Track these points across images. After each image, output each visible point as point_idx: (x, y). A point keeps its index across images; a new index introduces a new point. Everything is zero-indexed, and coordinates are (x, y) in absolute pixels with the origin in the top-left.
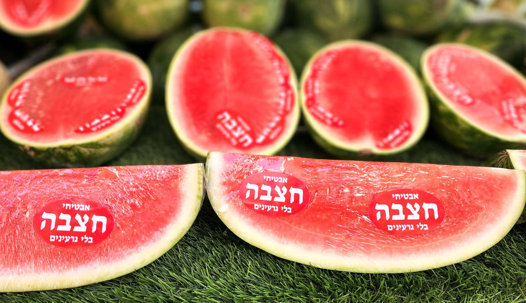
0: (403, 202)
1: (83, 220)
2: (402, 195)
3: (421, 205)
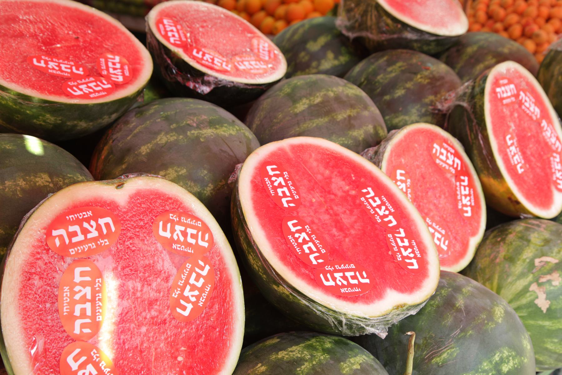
0: (79, 222)
2: (76, 215)
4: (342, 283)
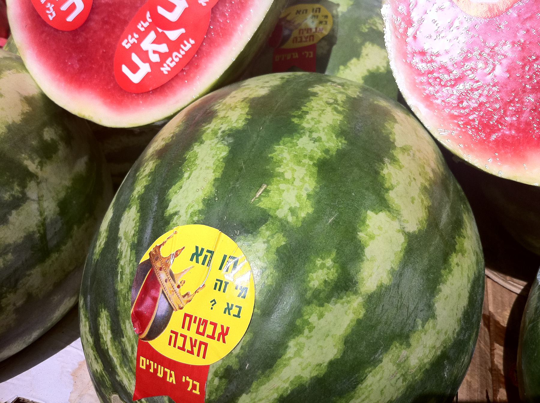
1: (155, 52)
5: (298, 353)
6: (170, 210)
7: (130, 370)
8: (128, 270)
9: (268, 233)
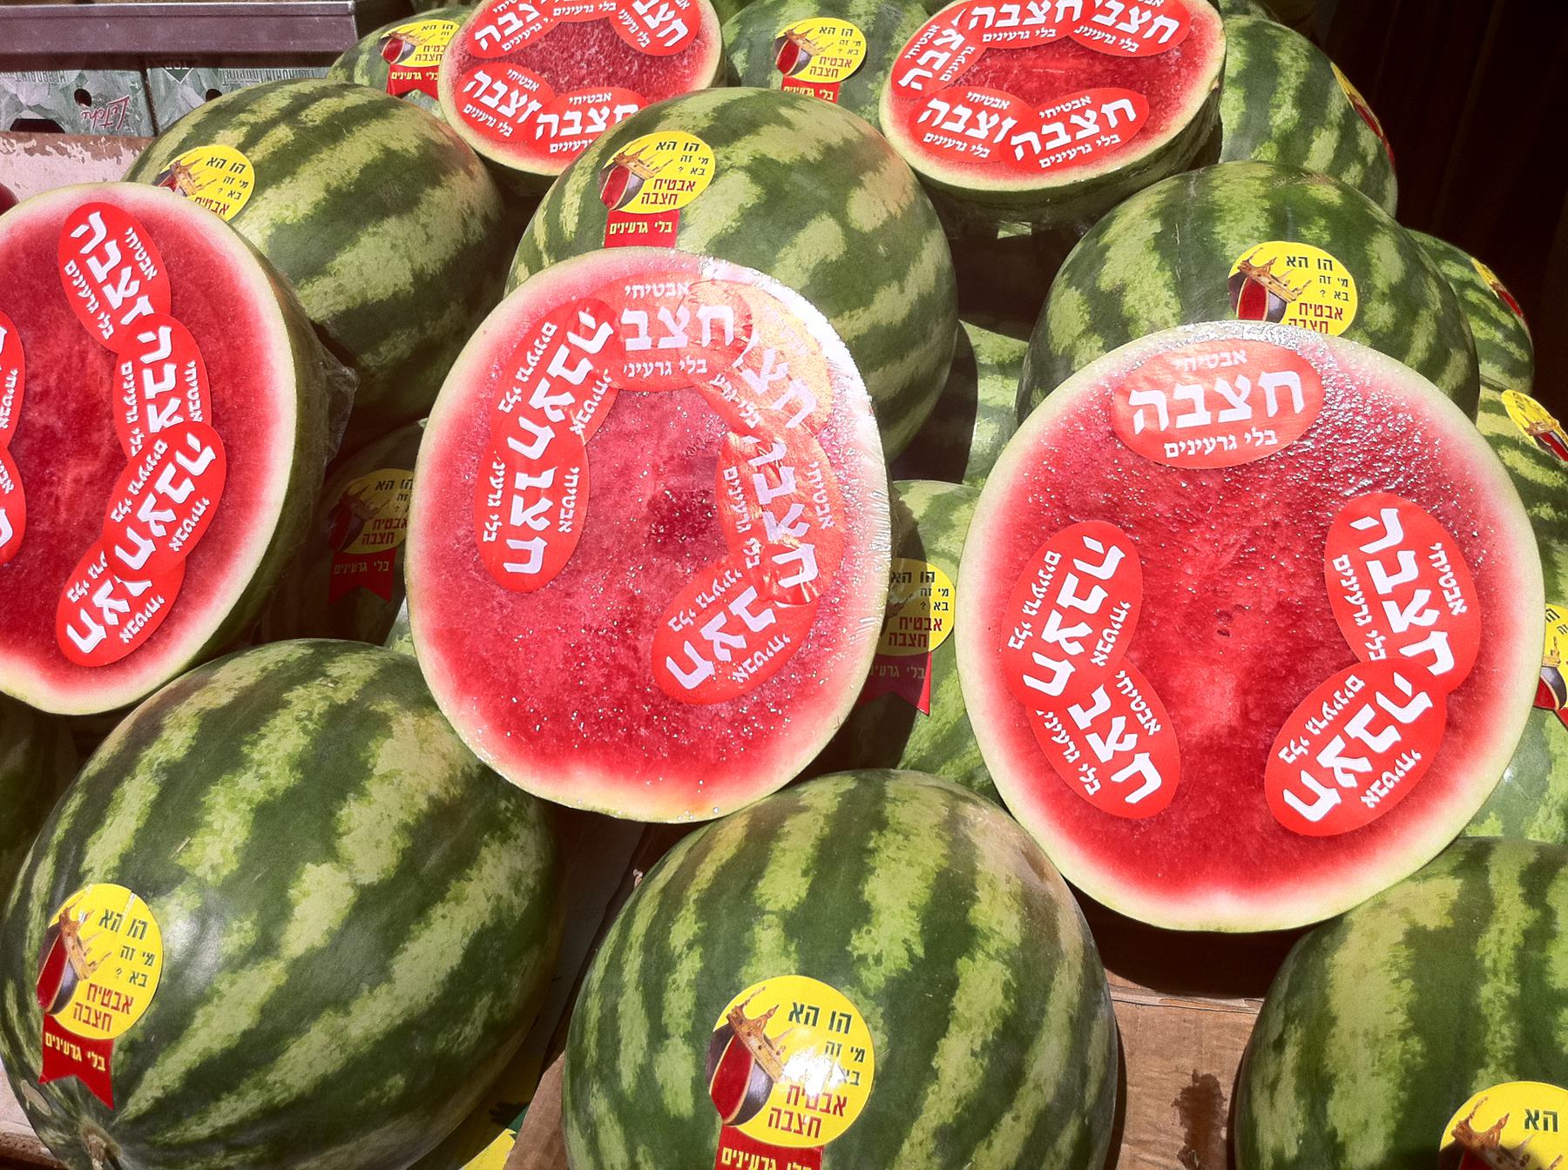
3: (1342, 791)
4: (131, 279)
5: (206, 1024)
6: (85, 865)
7: (37, 1049)
8: (36, 935)
9: (183, 894)
